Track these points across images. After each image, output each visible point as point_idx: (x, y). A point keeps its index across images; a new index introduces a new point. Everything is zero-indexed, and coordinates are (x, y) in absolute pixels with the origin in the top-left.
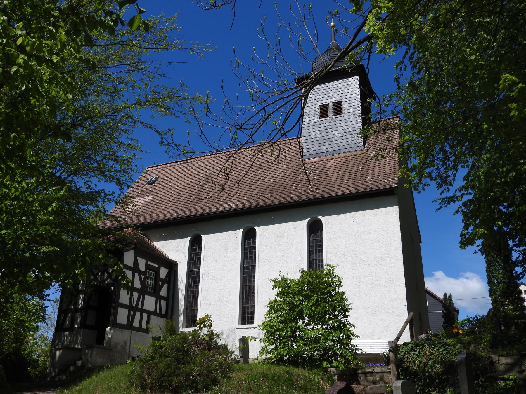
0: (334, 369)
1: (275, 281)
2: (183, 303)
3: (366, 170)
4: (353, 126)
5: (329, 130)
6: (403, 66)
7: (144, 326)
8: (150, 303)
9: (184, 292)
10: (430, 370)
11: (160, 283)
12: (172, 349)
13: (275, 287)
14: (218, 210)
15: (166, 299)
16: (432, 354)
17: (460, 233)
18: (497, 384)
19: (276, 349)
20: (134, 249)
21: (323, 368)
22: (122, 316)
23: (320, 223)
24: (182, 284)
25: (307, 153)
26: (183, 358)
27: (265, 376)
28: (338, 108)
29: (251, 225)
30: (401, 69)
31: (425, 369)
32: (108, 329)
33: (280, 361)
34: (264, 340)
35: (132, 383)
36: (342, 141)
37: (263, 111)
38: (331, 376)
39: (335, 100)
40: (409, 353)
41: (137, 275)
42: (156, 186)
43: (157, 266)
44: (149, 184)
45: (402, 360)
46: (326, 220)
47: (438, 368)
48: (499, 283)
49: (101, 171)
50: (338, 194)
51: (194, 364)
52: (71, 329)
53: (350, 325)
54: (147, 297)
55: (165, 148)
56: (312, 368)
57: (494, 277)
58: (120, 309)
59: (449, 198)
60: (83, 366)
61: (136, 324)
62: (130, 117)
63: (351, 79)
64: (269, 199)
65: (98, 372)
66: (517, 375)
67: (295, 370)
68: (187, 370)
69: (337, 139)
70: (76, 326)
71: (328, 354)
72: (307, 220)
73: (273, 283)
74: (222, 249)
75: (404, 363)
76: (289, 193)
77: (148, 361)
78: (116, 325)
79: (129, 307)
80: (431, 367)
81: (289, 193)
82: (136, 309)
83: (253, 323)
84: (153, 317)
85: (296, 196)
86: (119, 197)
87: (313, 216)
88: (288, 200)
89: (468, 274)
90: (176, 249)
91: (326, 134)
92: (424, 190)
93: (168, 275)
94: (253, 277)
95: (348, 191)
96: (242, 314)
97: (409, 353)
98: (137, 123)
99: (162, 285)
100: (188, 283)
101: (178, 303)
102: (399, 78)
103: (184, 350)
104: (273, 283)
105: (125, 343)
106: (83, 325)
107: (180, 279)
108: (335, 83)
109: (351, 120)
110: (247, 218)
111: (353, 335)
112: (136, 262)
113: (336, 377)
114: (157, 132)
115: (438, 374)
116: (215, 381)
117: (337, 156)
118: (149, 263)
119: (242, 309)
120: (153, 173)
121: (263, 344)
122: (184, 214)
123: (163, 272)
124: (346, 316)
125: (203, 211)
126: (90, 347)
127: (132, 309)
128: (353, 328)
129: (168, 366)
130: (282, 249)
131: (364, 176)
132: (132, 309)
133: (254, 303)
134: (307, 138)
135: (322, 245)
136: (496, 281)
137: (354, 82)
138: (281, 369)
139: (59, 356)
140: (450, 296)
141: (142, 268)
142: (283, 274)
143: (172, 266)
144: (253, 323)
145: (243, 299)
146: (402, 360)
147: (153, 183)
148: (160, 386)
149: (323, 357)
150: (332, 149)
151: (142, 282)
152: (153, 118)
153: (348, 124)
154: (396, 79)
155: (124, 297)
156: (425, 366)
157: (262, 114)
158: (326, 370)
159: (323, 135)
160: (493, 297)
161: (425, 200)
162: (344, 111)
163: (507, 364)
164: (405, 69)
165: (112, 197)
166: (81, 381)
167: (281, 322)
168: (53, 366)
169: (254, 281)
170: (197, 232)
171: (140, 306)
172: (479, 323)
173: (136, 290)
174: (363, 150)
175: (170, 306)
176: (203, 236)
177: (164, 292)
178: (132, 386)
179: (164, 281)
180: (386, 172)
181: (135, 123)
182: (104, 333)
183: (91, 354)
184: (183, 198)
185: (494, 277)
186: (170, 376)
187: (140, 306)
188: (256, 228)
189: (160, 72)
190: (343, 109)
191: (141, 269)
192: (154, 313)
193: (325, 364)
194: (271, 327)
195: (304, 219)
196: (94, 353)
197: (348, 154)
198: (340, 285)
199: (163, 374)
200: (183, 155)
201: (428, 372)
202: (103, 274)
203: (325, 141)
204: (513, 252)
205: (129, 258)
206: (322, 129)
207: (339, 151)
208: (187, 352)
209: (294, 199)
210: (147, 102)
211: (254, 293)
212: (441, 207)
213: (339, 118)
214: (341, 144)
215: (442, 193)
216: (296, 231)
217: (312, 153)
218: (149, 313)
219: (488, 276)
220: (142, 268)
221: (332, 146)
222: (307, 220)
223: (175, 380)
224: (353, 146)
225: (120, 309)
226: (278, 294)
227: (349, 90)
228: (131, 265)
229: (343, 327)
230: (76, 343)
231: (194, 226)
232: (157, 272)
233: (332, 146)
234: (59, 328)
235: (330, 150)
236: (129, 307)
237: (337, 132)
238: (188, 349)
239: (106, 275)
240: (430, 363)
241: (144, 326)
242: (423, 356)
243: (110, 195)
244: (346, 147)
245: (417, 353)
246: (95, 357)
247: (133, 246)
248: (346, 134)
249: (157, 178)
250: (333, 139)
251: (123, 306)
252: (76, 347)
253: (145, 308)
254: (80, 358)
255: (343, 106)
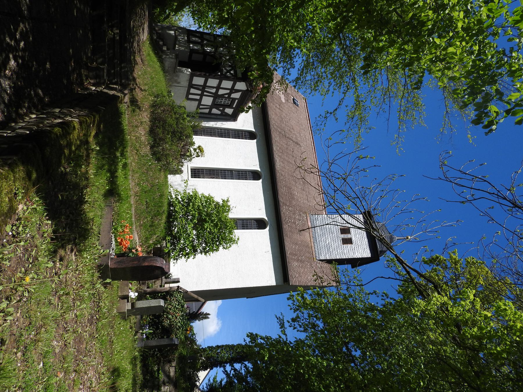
0: (164, 245)
1: (228, 201)
2: (207, 125)
3: (302, 261)
4: (334, 252)
5: (331, 235)
6: (385, 297)
7: (191, 96)
8: (207, 101)
9: (215, 126)
10: (165, 316)
11: (221, 109)
12: (182, 128)
13: (223, 201)
14: (274, 152)
15: (210, 113)
16: (176, 318)
17: (258, 333)
18: (155, 365)
19: (179, 202)
20: (248, 90)
21: (166, 237)
22: (199, 81)
23: (264, 228)
24: (220, 125)
25: (314, 218)
26: (176, 136)
27: (161, 196)
28: (348, 241)
29: (263, 177)
30: (383, 296)
31: (165, 312)
32: (190, 70)
33: (170, 204)
34: (185, 193)
35: (157, 96)
36: (323, 244)
37: (355, 196)
38: (160, 243)
39: (354, 239)
40: (177, 300)
41: (228, 91)
42: (291, 106)
43: (234, 106)
44: (294, 99)
45: (171, 295)
46: (266, 232)
47: (166, 323)
48: (217, 354)
49: (307, 66)
50: (285, 242)
51: (171, 144)
52: (189, 41)
53: (195, 255)
54: (211, 99)
55: (324, 115)
56: (166, 229)
57: (222, 350)
58: (204, 79)
59: (283, 324)
60: (163, 51)
61: (192, 91)
62: (348, 89)
63: (369, 251)
64: (282, 191)
65: (161, 67)
66: (162, 380)
67: (164, 217)
68: (168, 140)
69: (325, 240)
70: (191, 45)
71: (175, 239)
72: (266, 218)
73: (226, 200)
74: (245, 154)
75: (170, 297)
76: (286, 205)
77: (173, 110)
78: (192, 76)
79: (205, 86)
80: (167, 317)
81: (286, 205)
82: (203, 91)
83: (192, 177)
84: (197, 103)
85: (284, 210)
86: (287, 79)
87: (269, 223)
88: (281, 204)
89: (220, 322)
90: (246, 121)
91: (328, 232)
92: (291, 309)
93: (227, 115)
94: (224, 177)
95: (287, 248)
96: (198, 169)
97: (177, 300)
98: (344, 95)
99: (220, 110)
100: (221, 129)
101: (207, 122)
102: (376, 294)
103: (181, 137)
104: (226, 200)
105: (179, 83)
106: (192, 51)
107: (224, 123)
108: (366, 240)
109: (338, 251)
110: (268, 173)
111: (188, 258)
112: (237, 91)
113: (159, 246)
114: (336, 109)
115: (162, 322)
116: (159, 160)
117: (312, 240)
118: (237, 101)
119: (202, 169)
120: (301, 102)
121: (182, 192)
122: (271, 126)
123: (229, 111)
124: (201, 252)
125: (274, 141)
126: (177, 56)
127: (203, 88)
128: (192, 257)
129: (171, 126)
130: (247, 200)
131: (298, 260)
132: (203, 88)
133: (206, 178)
134: (326, 218)
135: (247, 229)
136: (219, 351)
137: (366, 253)
138: (165, 208)
139: (170, 34)
140: (208, 318)
141: (233, 96)
142: (234, 209)
143: (234, 117)
144: (192, 177)
145: (209, 170)
146: (171, 295)
147: (294, 103)
148: (155, 119)
149: (174, 237)
150: (317, 236)
151: (222, 96)
152: (346, 106)
153: (336, 248)
154: (375, 292)
155: (213, 82)
156: (168, 313)
157: (353, 195)
158: (164, 239)
159: (328, 230)
160: (207, 349)
161: (281, 304)
162: (345, 245)
163: (169, 372)
164: (382, 299)
165: (286, 73)
166: (155, 54)
167: (199, 206)
168: (163, 28)
169: (222, 178)
170: (258, 137)
171: (205, 93)
172: (191, 340)
173: (217, 91)
174: (316, 259)
175: (205, 116)
176: (255, 140)
177: (215, 111)
178: (155, 97)
179: (223, 111)
180: (301, 275)
181: (343, 93)
182: (187, 67)
183: (172, 58)
184: (283, 125)
185: (222, 350)
186: (163, 126)
187: (205, 93)
188: (261, 180)
189: (381, 112)
190: (347, 245)
191: (232, 95)
192: (200, 104)
193: (168, 238)
194: (196, 198)
195: (267, 216)
196: (172, 60)
197: (313, 248)
198: (224, 248)
199: (165, 122)
200: (316, 128)
201: (164, 315)
202: (230, 66)
203: (323, 231)
204: (240, 365)
205: (241, 86)
206: (332, 230)
207: (315, 242)
208: (180, 139)
209: (281, 209)
210: (358, 102)
211: (213, 178)
212: (278, 319)
213: (340, 242)
214: (321, 243)
215: (288, 322)
216: (258, 209)
217: (315, 222)
218: (200, 100)
219: (223, 346)
220: (233, 96)
221: (320, 237)
222: (266, 218)
223: (160, 131)
224: (320, 252)
225: (204, 79)
226: (218, 203)
227: (360, 248)
228: (236, 88)
229: (194, 250)
230: (179, 46)
231: (263, 135)
232: (230, 106)
233: (320, 237)
234: (189, 33)
235: (317, 235)
236: (205, 86)
237: (330, 241)
238: (181, 139)
239: (228, 69)
240: (170, 316)
241: (191, 96)
242: (175, 311)
243: (288, 72)
244: (319, 247)
245: (177, 306)
246: (170, 60)
247: (249, 89)
248: (328, 247)
249: (298, 106)
250: (324, 237)
251: (206, 82)
252: (177, 46)
253: (204, 98)
254: (168, 49)
255: (349, 245)
